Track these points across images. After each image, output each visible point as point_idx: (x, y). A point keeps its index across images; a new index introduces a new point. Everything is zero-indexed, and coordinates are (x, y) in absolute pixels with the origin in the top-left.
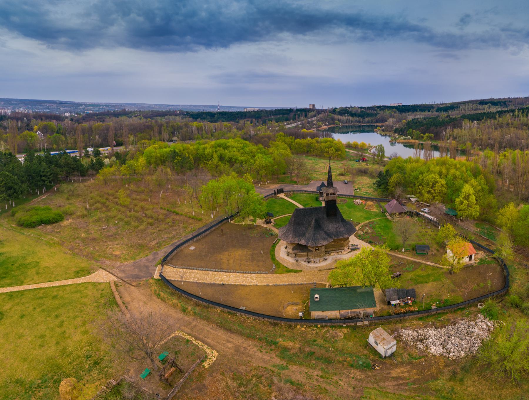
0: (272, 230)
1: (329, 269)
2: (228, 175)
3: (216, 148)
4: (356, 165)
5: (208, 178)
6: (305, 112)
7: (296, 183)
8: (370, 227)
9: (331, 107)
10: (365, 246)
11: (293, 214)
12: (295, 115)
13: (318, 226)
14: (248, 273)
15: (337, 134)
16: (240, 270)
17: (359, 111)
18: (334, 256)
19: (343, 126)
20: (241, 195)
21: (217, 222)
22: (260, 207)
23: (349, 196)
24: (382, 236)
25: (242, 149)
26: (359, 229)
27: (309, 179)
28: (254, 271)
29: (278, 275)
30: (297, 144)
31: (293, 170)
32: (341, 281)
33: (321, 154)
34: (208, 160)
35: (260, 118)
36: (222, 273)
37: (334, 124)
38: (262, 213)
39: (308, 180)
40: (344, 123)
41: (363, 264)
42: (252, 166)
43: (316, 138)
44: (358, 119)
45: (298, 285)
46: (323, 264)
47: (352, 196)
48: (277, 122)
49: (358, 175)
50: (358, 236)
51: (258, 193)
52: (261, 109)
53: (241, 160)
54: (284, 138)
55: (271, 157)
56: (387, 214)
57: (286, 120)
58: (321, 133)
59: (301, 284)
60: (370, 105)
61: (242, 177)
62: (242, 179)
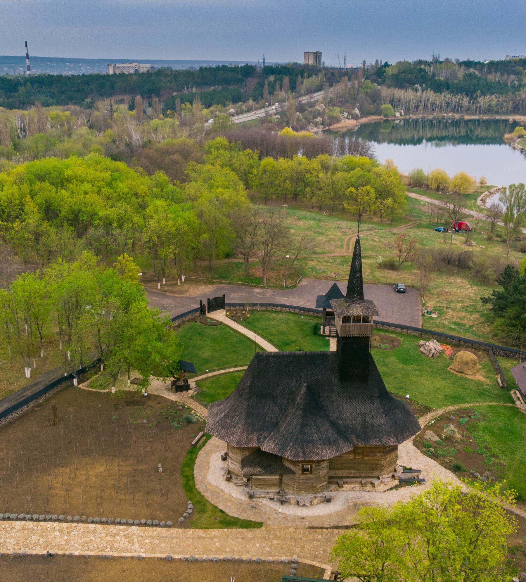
0: (190, 409)
1: (337, 527)
2: (71, 259)
3: (32, 183)
4: (436, 242)
5: (15, 267)
6: (289, 76)
7: (258, 282)
8: (459, 425)
9: (371, 62)
10: (438, 477)
11: (250, 366)
12: (262, 85)
13: (315, 406)
14: (120, 523)
15: (385, 145)
16: (100, 515)
17: (461, 73)
18: (352, 494)
19: (406, 121)
20: (108, 313)
21: (41, 387)
22: (159, 345)
23: (408, 328)
24: (494, 456)
25: (109, 185)
26: (429, 427)
27: (297, 274)
28: (136, 517)
29: (200, 532)
30: (265, 171)
31: (252, 245)
32: (368, 564)
33: (335, 204)
34: (9, 219)
35: (158, 95)
36: (49, 524)
37: (377, 112)
38: (165, 363)
39: (294, 275)
40: (407, 112)
41: (432, 523)
42: (138, 235)
43: (321, 157)
44: (455, 99)
45: (250, 562)
46: (319, 511)
47: (415, 329)
48: (208, 106)
49: (439, 271)
50: (423, 446)
51: (156, 309)
52: (158, 66)
53: (107, 217)
54: (227, 154)
55: (192, 208)
56: (515, 394)
57: (235, 101)
58: (337, 142)
59: (258, 562)
60: (500, 57)
61: (110, 264)
62: (111, 270)
